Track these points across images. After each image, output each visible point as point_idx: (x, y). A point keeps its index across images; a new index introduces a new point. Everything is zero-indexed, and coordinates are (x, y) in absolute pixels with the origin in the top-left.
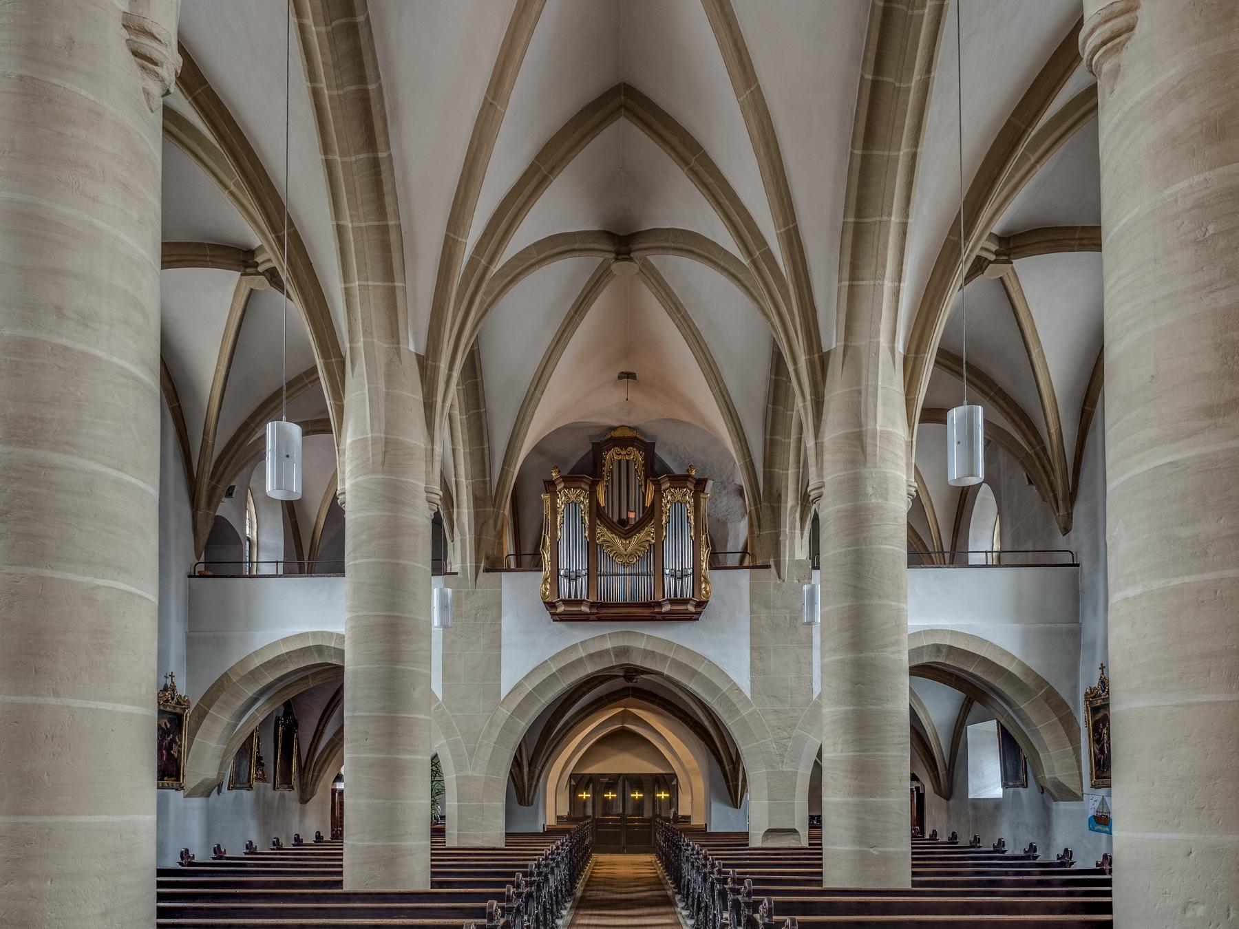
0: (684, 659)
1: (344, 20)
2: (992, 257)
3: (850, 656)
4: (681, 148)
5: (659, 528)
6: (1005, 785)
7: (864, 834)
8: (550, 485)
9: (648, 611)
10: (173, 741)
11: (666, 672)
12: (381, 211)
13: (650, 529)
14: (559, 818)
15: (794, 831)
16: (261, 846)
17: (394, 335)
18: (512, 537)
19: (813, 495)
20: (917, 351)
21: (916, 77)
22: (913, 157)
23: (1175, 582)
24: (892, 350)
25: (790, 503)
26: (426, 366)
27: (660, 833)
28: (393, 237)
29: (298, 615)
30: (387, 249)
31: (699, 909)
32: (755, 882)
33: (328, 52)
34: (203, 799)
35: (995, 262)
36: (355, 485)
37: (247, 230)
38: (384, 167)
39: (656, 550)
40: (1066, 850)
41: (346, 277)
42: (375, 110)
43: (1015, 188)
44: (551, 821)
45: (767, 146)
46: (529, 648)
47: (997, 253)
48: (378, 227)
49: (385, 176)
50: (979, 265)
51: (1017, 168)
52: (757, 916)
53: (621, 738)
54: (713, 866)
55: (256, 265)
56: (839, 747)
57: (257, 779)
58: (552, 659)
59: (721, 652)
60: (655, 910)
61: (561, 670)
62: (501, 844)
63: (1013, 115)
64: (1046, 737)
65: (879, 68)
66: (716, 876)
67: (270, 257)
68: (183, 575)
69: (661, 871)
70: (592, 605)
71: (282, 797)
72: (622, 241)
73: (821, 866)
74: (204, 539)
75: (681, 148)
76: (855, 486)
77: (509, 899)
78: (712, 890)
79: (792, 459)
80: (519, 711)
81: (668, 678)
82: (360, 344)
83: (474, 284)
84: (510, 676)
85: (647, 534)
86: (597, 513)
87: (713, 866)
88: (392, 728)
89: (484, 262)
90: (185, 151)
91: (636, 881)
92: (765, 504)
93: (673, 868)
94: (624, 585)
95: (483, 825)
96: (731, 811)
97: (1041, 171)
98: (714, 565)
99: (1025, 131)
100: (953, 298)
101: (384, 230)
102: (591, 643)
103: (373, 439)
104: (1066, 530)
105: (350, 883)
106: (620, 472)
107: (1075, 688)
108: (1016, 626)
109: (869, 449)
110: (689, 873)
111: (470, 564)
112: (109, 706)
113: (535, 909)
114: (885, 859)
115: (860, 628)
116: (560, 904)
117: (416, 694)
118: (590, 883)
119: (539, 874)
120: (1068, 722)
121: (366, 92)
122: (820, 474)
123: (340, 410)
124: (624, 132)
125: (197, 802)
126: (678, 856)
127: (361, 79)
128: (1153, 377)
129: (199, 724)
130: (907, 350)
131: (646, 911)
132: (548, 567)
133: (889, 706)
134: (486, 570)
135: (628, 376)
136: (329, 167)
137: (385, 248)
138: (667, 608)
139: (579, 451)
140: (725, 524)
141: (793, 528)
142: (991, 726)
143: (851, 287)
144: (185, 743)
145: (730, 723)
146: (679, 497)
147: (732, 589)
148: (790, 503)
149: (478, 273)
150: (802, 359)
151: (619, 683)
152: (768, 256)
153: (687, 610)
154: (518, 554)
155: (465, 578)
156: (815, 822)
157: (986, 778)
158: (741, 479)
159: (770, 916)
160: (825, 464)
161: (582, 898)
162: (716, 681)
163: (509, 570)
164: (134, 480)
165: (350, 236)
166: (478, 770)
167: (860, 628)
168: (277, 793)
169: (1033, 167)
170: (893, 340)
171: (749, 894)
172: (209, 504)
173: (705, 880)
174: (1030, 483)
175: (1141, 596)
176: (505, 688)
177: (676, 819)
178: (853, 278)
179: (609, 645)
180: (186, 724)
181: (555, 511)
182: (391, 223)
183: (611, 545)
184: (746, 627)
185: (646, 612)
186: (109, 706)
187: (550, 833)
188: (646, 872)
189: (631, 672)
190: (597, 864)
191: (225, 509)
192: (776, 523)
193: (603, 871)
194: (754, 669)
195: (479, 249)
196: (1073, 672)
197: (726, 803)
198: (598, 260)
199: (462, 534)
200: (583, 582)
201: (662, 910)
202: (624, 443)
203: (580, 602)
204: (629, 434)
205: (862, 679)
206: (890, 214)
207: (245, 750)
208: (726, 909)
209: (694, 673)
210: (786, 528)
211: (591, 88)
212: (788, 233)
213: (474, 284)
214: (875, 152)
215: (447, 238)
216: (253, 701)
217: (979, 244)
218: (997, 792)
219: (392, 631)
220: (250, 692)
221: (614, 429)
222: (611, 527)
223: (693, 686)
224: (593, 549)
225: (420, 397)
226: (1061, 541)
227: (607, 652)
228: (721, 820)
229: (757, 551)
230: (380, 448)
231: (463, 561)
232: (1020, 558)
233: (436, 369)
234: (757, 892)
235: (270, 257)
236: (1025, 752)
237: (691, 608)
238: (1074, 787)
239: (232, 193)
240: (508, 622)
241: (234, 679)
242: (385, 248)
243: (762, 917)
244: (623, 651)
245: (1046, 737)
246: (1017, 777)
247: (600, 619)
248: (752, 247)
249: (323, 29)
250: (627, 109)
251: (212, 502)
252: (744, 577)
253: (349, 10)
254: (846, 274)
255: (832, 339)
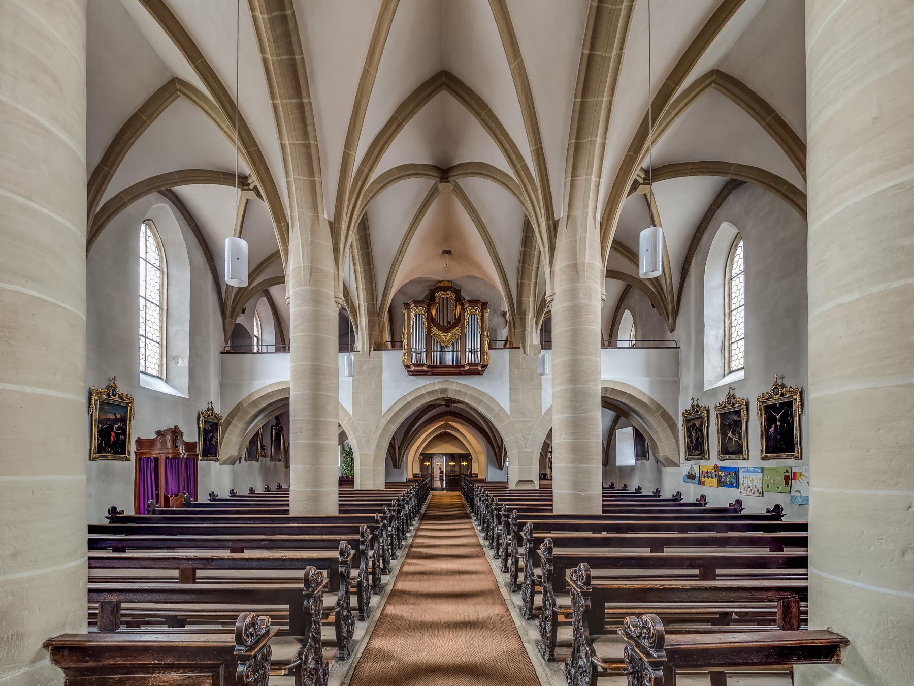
0: (476, 395)
1: (278, 13)
2: (642, 181)
3: (569, 387)
4: (476, 107)
5: (463, 327)
6: (637, 460)
7: (578, 484)
8: (407, 305)
9: (457, 370)
10: (213, 436)
11: (466, 401)
12: (306, 135)
13: (459, 328)
14: (415, 475)
15: (532, 481)
16: (259, 489)
17: (315, 208)
18: (388, 335)
19: (548, 300)
20: (608, 220)
21: (614, 53)
22: (611, 103)
23: (897, 284)
24: (595, 218)
25: (530, 316)
26: (334, 227)
27: (460, 480)
28: (313, 151)
29: (274, 372)
30: (310, 158)
31: (484, 522)
32: (519, 510)
33: (270, 31)
34: (231, 466)
35: (643, 184)
36: (295, 292)
37: (245, 167)
38: (307, 108)
39: (462, 338)
40: (702, 496)
41: (287, 175)
42: (300, 72)
43: (663, 130)
44: (410, 476)
45: (527, 98)
46: (397, 388)
47: (644, 179)
48: (305, 145)
49: (307, 114)
50: (636, 185)
51: (668, 113)
52: (522, 534)
53: (444, 436)
54: (492, 500)
55: (249, 185)
56: (563, 437)
57: (261, 456)
58: (408, 394)
59: (492, 393)
60: (461, 521)
61: (413, 400)
62: (382, 487)
63: (667, 79)
64: (661, 434)
65: (593, 47)
66: (494, 506)
67: (254, 181)
68: (218, 352)
69: (464, 500)
70: (429, 367)
71: (275, 465)
72: (444, 171)
73: (552, 500)
74: (229, 334)
75: (476, 107)
76: (573, 293)
77: (377, 522)
78: (492, 513)
79: (532, 293)
80: (391, 421)
81: (468, 405)
82: (296, 214)
83: (360, 188)
84: (386, 405)
85: (457, 331)
86: (431, 320)
87: (488, 496)
88: (316, 426)
89: (366, 170)
90: (199, 108)
91: (452, 506)
92: (518, 315)
93: (471, 501)
94: (443, 358)
95: (370, 477)
96: (498, 471)
97: (678, 121)
98: (490, 348)
99: (674, 89)
100: (624, 201)
101: (308, 147)
102: (428, 387)
103: (304, 267)
104: (672, 330)
105: (296, 509)
106: (444, 303)
107: (677, 410)
108: (647, 378)
109: (581, 273)
110: (478, 503)
111: (366, 346)
112: (18, 388)
113: (396, 523)
114: (588, 498)
115: (576, 374)
116: (411, 519)
117: (330, 408)
118: (430, 507)
119: (399, 505)
120: (673, 426)
121: (294, 60)
122: (553, 288)
123: (287, 252)
124: (445, 99)
125: (227, 468)
126: (472, 494)
127: (291, 52)
128: (876, 118)
129: (227, 428)
130: (602, 219)
131: (456, 521)
132: (406, 348)
133: (591, 414)
134: (375, 350)
135: (447, 252)
136: (275, 106)
137: (309, 158)
138: (467, 368)
139: (421, 293)
140: (495, 330)
141: (532, 328)
142: (630, 430)
143: (572, 181)
144: (219, 438)
145: (499, 427)
146: (473, 311)
147: (500, 359)
148: (530, 316)
149: (363, 176)
150: (543, 224)
151: (443, 409)
152: (525, 168)
153: (478, 370)
154: (393, 342)
155: (364, 353)
156: (545, 478)
157: (626, 455)
158: (506, 307)
159: (531, 534)
160: (556, 283)
161: (425, 514)
162: (492, 406)
163: (387, 349)
164: (45, 211)
165: (288, 150)
166: (371, 451)
167: (576, 374)
168: (273, 463)
169: (673, 118)
170: (595, 212)
171: (516, 519)
172: (232, 316)
173: (487, 507)
174: (653, 307)
175: (858, 300)
176: (384, 410)
177: (471, 475)
178: (573, 176)
179: (437, 387)
180: (220, 428)
181: (409, 319)
182: (312, 142)
183: (439, 336)
184: (507, 378)
185: (456, 370)
186: (18, 388)
187: (409, 481)
188: (456, 501)
189: (449, 402)
190: (433, 496)
191: (241, 320)
192: (523, 325)
193: (436, 500)
194: (511, 400)
195: (364, 162)
196: (676, 402)
197: (495, 467)
198: (432, 182)
199: (362, 331)
200: (424, 355)
201: (464, 521)
202: (445, 289)
203: (422, 365)
204: (447, 284)
205: (576, 399)
206: (596, 136)
207: (253, 442)
208: (500, 524)
209: (481, 402)
210: (528, 329)
211: (425, 72)
212: (537, 150)
213: (360, 188)
214: (588, 100)
215: (344, 152)
216: (256, 416)
217: (636, 174)
218: (632, 462)
219: (317, 376)
220: (253, 412)
221: (441, 282)
222: (439, 327)
223: (481, 409)
224: (429, 339)
225: (331, 245)
226: (669, 336)
227: (436, 391)
228: (493, 475)
229: (513, 340)
230: (308, 272)
231: (363, 345)
232: (647, 344)
233: (339, 229)
234: (520, 517)
235: (254, 181)
236: (648, 440)
237: (480, 368)
238: (676, 461)
239: (225, 132)
240: (386, 375)
241: (245, 405)
242: (309, 158)
243: (525, 534)
244: (444, 391)
245: (661, 434)
246: (644, 455)
247: (433, 374)
248: (516, 162)
249: (266, 16)
250: (446, 84)
251: (234, 315)
252: (506, 353)
253: (281, 6)
254: (569, 174)
255: (560, 213)
